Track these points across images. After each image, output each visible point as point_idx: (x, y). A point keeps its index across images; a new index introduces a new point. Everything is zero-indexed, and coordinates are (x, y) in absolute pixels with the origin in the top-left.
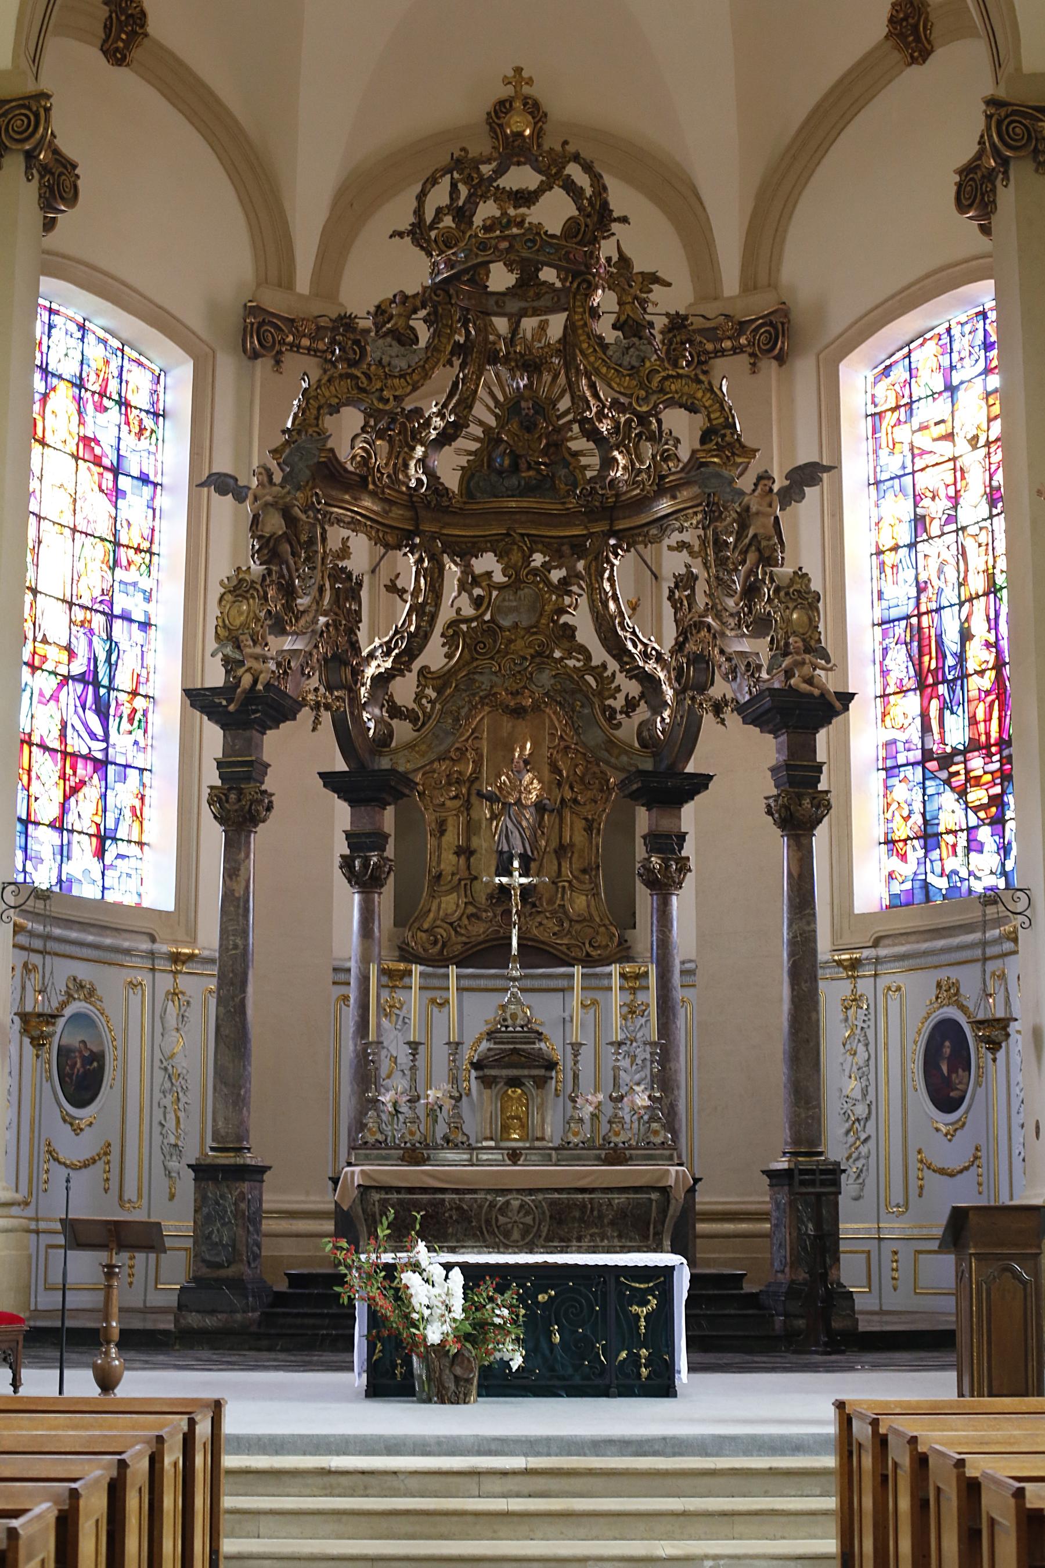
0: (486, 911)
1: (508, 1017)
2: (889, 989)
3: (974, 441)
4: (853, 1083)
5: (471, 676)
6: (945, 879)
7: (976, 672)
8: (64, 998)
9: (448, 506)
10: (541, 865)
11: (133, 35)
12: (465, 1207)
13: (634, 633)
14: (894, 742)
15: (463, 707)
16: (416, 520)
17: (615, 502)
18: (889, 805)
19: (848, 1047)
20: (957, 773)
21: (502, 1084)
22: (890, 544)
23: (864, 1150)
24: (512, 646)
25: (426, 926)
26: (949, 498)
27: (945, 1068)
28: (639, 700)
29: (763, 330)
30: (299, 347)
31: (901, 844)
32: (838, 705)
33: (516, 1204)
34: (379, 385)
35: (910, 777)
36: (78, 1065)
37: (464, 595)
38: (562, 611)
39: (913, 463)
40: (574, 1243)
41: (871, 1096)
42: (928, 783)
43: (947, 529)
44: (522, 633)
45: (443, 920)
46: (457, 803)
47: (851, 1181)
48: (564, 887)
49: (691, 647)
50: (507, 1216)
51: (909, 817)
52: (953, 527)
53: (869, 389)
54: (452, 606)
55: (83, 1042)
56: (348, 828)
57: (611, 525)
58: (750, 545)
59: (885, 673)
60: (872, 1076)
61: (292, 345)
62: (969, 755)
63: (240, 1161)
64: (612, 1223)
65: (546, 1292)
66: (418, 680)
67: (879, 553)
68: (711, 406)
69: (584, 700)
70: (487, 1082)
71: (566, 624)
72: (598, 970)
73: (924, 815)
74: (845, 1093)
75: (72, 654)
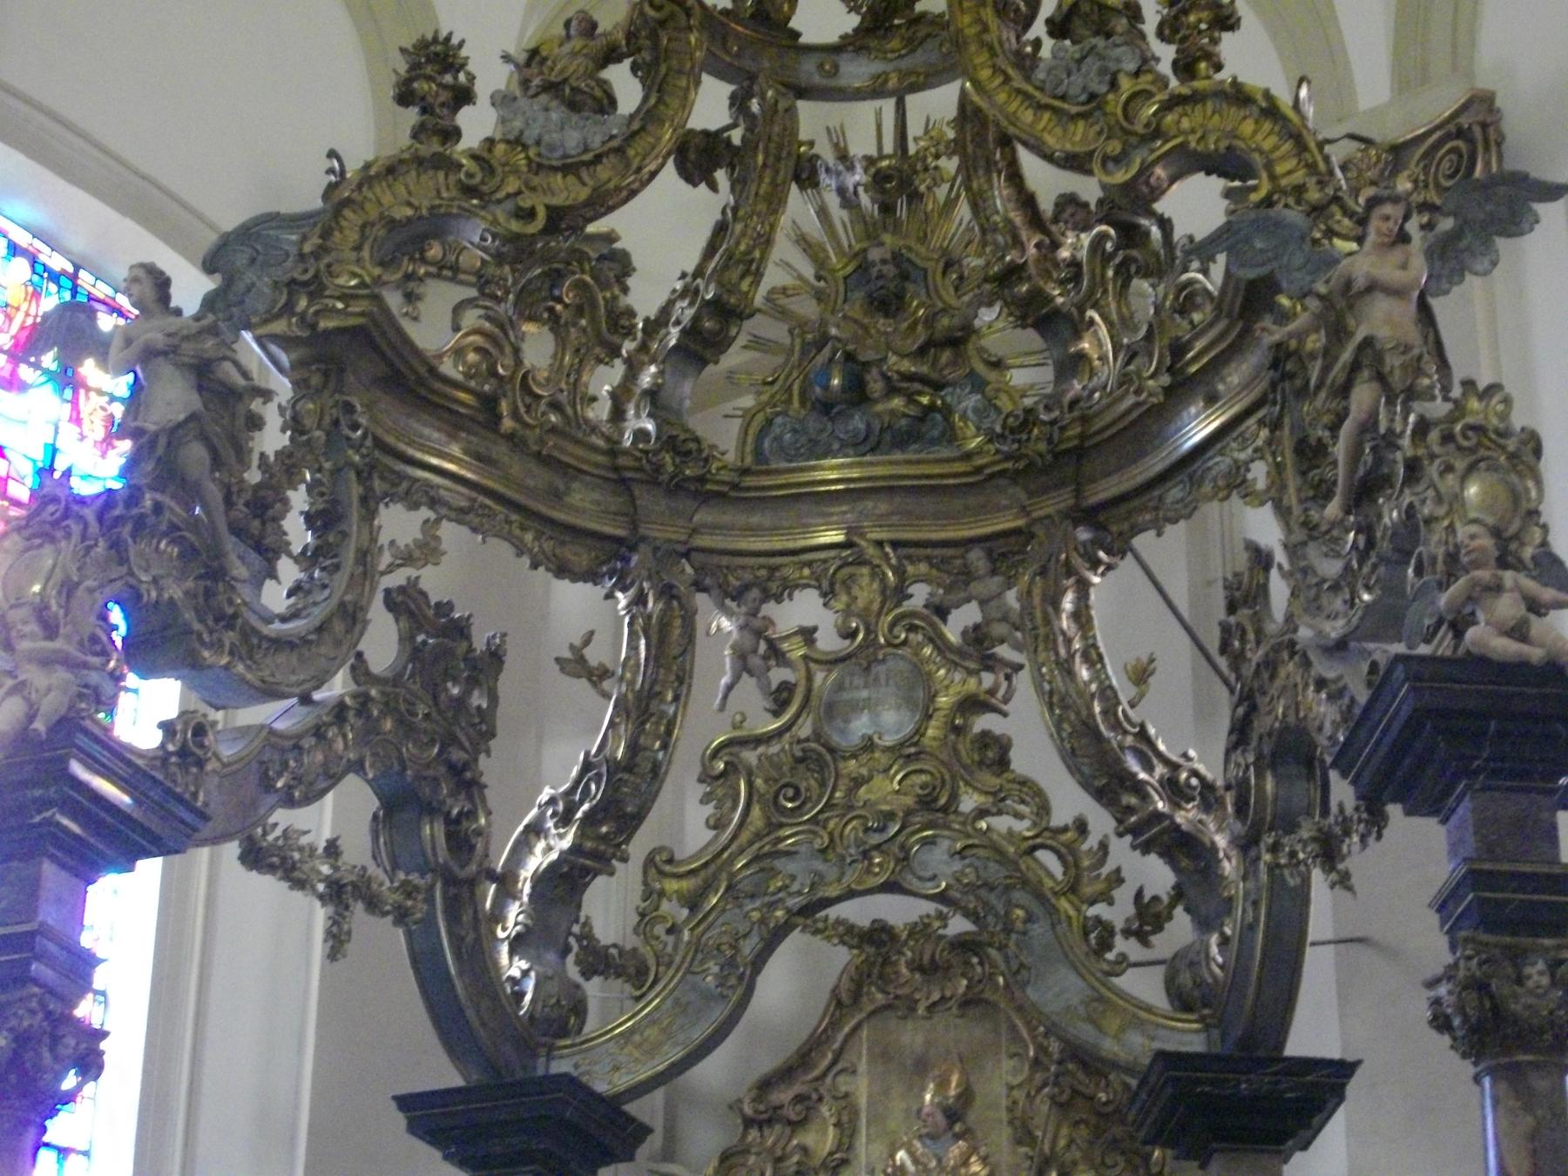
5: (766, 863)
9: (702, 480)
13: (1143, 735)
17: (1082, 437)
28: (1172, 906)
29: (1448, 146)
30: (455, 268)
34: (512, 185)
38: (973, 704)
44: (882, 759)
54: (722, 707)
57: (1078, 493)
58: (1355, 367)
61: (441, 265)
66: (645, 883)
68: (1276, 148)
69: (1037, 909)
71: (985, 734)
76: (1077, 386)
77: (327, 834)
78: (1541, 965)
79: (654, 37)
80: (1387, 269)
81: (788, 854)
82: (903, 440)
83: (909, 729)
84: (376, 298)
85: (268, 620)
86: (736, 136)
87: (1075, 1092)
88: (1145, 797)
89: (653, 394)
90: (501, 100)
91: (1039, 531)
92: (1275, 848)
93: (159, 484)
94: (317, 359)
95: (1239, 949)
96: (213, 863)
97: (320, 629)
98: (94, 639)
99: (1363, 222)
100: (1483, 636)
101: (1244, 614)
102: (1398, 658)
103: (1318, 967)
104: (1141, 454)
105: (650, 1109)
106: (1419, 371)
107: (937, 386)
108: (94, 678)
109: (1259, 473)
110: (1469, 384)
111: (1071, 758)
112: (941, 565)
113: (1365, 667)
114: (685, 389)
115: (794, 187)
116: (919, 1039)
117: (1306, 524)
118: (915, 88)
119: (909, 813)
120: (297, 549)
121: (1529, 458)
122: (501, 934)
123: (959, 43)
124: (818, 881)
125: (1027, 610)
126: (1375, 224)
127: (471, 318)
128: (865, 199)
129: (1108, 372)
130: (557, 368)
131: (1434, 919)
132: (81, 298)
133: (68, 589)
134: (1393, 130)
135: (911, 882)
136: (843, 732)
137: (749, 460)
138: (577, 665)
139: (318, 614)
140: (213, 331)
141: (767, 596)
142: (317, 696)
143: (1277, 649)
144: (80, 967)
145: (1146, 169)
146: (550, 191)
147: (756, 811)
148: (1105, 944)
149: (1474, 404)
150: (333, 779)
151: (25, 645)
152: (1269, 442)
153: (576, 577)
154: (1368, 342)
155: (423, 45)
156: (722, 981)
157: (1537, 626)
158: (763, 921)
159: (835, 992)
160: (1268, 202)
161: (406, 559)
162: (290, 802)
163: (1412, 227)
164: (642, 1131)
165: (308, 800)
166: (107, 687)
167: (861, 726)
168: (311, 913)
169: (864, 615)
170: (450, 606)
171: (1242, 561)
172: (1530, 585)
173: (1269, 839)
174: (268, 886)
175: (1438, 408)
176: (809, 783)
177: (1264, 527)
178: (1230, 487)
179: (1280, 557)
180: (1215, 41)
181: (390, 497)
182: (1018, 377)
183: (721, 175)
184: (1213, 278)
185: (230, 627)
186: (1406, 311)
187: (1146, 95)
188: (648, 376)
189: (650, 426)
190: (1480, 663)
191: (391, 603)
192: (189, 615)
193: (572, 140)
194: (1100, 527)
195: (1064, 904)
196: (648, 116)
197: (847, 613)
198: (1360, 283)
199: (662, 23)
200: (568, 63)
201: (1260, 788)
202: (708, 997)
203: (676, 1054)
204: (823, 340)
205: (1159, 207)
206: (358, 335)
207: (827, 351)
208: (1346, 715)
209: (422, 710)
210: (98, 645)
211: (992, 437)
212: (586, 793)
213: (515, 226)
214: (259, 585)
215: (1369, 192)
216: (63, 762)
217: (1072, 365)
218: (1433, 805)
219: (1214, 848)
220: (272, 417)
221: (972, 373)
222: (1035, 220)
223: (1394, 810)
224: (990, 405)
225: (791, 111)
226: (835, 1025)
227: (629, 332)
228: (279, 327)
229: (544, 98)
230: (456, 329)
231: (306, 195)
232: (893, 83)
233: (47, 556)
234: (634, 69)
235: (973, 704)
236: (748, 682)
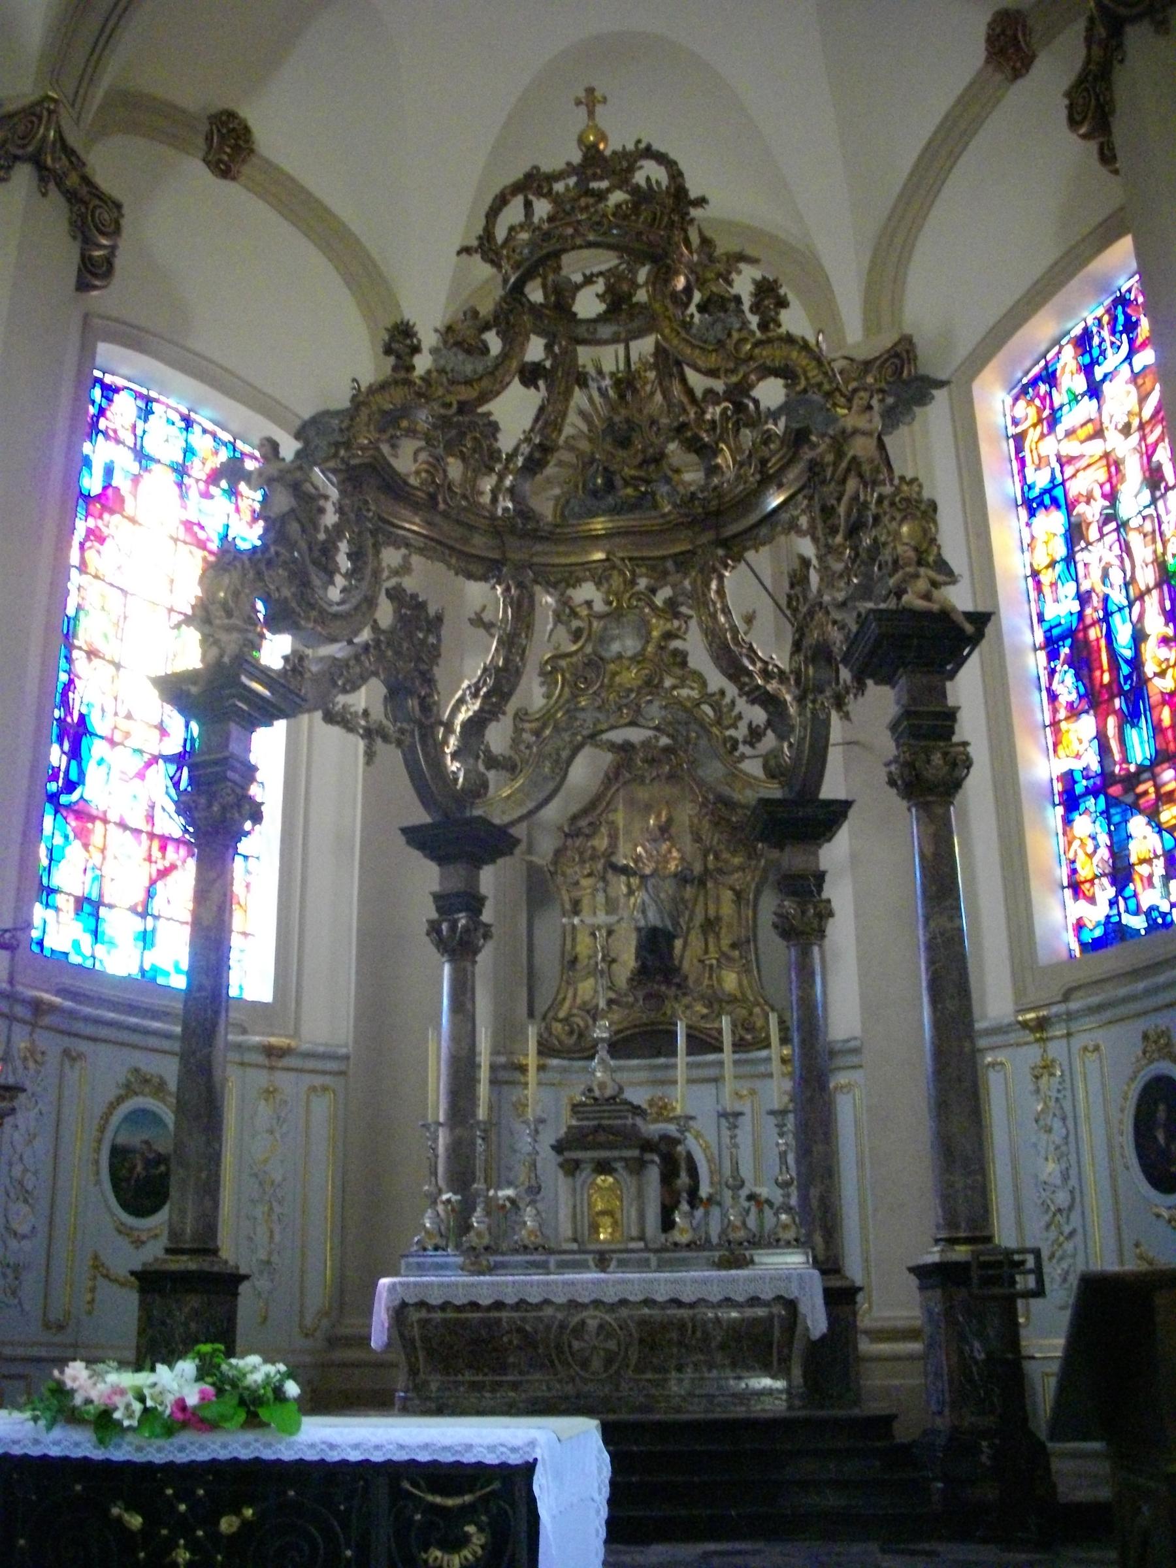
0: (626, 995)
2: (1085, 1049)
3: (1126, 430)
6: (1143, 917)
7: (1156, 674)
9: (536, 530)
13: (751, 648)
16: (502, 547)
18: (1070, 843)
19: (1042, 1123)
20: (1146, 793)
22: (1047, 561)
23: (1069, 1246)
26: (1104, 496)
27: (1161, 1137)
32: (969, 628)
33: (592, 1324)
34: (440, 392)
36: (139, 1168)
37: (561, 629)
38: (669, 636)
39: (1062, 472)
40: (674, 1374)
41: (1073, 1182)
42: (1112, 811)
43: (1106, 529)
44: (626, 663)
45: (579, 1008)
47: (1055, 1286)
49: (809, 641)
51: (1095, 852)
52: (1113, 525)
56: (436, 888)
58: (848, 470)
59: (1053, 697)
60: (1073, 1158)
62: (1158, 769)
63: (206, 1267)
64: (722, 1347)
65: (238, 1513)
73: (1110, 848)
75: (164, 732)
78: (939, 755)
80: (861, 422)
81: (583, 709)
83: (639, 648)
84: (378, 449)
86: (548, 364)
87: (720, 817)
90: (434, 351)
91: (700, 551)
92: (814, 701)
94: (349, 479)
95: (797, 749)
96: (311, 721)
98: (250, 618)
99: (850, 400)
100: (911, 599)
101: (798, 589)
102: (871, 611)
103: (835, 757)
105: (519, 831)
107: (648, 482)
108: (250, 636)
109: (804, 521)
110: (902, 478)
112: (653, 568)
113: (855, 614)
114: (527, 487)
115: (577, 389)
116: (647, 796)
117: (827, 545)
118: (635, 338)
119: (640, 688)
120: (343, 570)
121: (931, 512)
122: (447, 751)
123: (654, 318)
124: (597, 722)
126: (856, 401)
128: (611, 393)
129: (730, 474)
131: (889, 733)
132: (238, 455)
133: (236, 594)
134: (862, 354)
135: (641, 721)
136: (607, 650)
137: (558, 520)
138: (478, 621)
140: (300, 468)
141: (568, 586)
143: (813, 606)
144: (250, 772)
145: (746, 376)
147: (567, 690)
148: (735, 747)
149: (905, 488)
151: (218, 622)
152: (808, 506)
154: (854, 458)
157: (936, 594)
159: (607, 775)
160: (805, 391)
161: (396, 573)
162: (345, 691)
163: (875, 402)
164: (516, 842)
166: (256, 639)
167: (615, 647)
168: (356, 746)
169: (616, 594)
171: (796, 564)
172: (932, 574)
173: (811, 697)
174: (336, 731)
175: (887, 489)
176: (591, 675)
177: (807, 548)
179: (815, 562)
180: (777, 314)
182: (688, 477)
183: (541, 383)
184: (778, 428)
185: (313, 609)
186: (872, 443)
188: (508, 481)
189: (510, 505)
191: (389, 594)
192: (294, 605)
193: (468, 369)
195: (715, 730)
196: (505, 356)
197: (608, 593)
198: (849, 429)
199: (511, 311)
200: (466, 330)
202: (545, 779)
203: (531, 805)
204: (592, 461)
205: (755, 393)
208: (847, 638)
210: (252, 620)
211: (675, 506)
213: (442, 411)
214: (326, 589)
215: (854, 385)
216: (238, 676)
218: (888, 680)
220: (330, 508)
223: (870, 682)
224: (675, 490)
227: (499, 460)
231: (342, 401)
232: (623, 336)
235: (669, 636)
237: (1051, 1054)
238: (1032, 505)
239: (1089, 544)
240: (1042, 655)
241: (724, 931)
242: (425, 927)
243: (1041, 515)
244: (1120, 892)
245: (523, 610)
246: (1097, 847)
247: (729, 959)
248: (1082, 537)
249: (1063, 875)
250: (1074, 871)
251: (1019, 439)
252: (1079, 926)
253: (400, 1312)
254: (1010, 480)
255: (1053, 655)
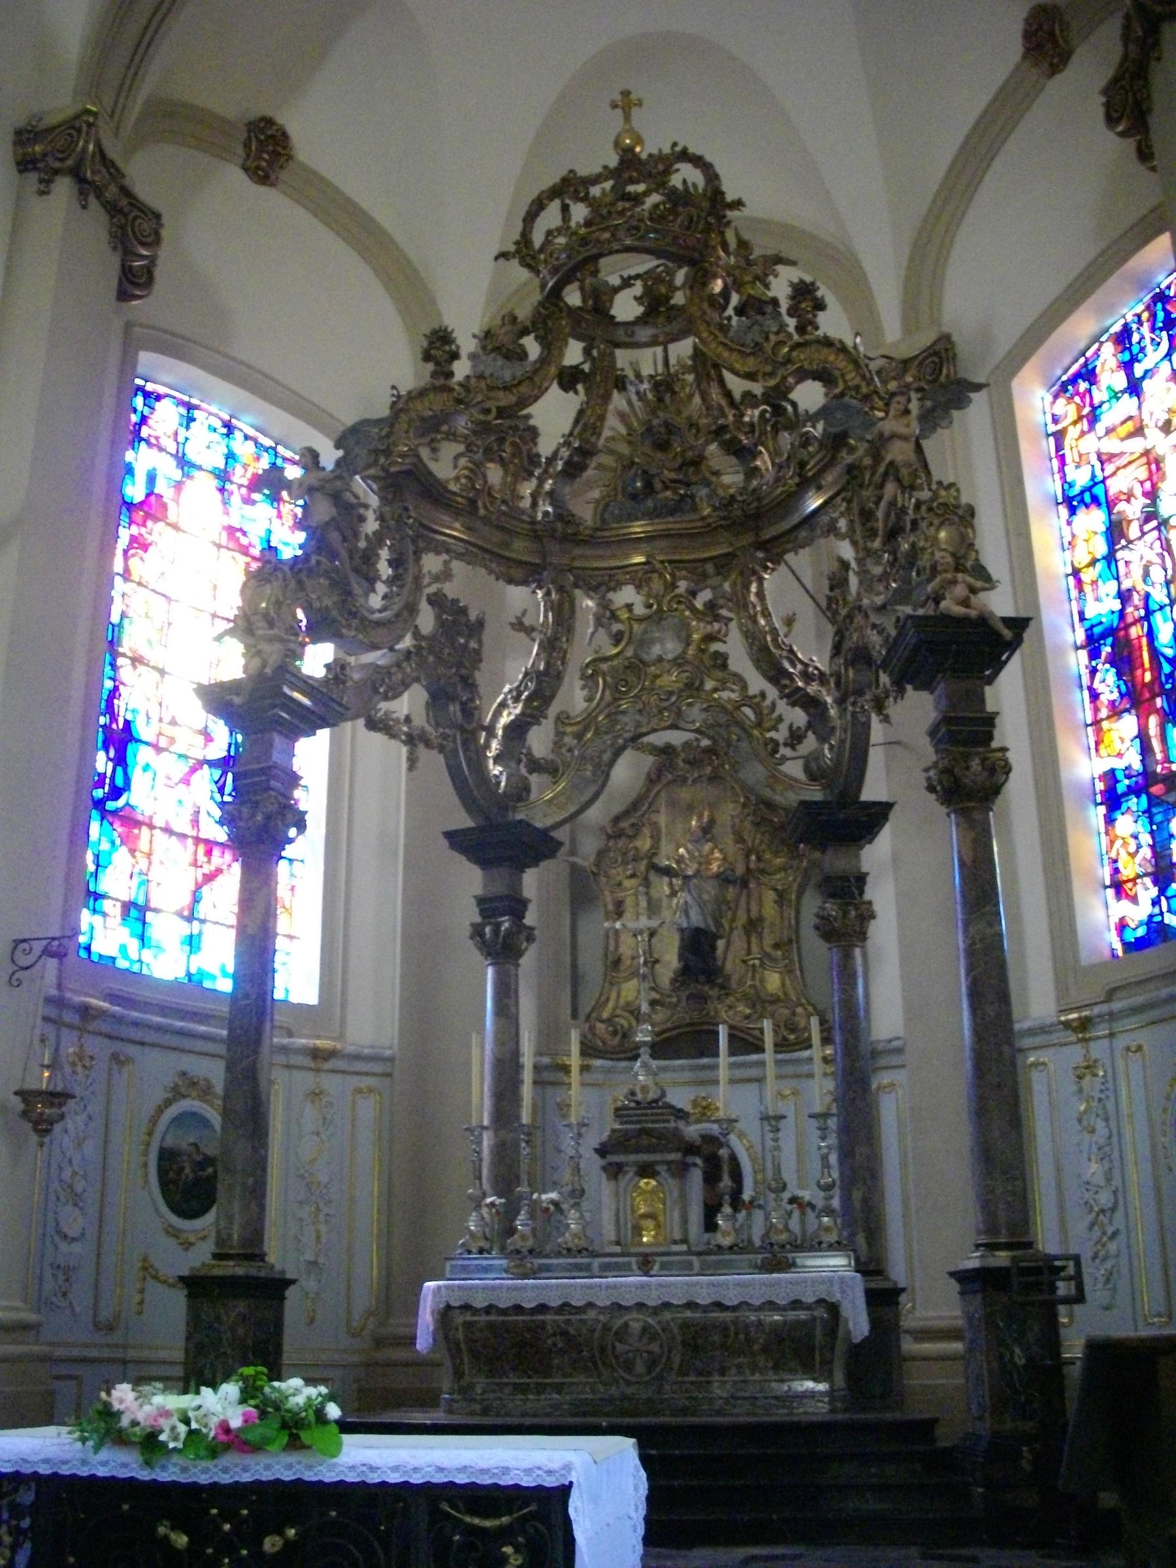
0: (670, 996)
1: (638, 1090)
2: (1128, 1049)
4: (1094, 1167)
8: (170, 1095)
9: (575, 534)
10: (728, 942)
11: (276, 155)
12: (572, 1332)
13: (791, 651)
14: (1112, 771)
15: (604, 751)
17: (758, 508)
18: (1112, 843)
19: (1085, 1123)
21: (631, 1174)
22: (1088, 559)
23: (1112, 1247)
24: (658, 682)
25: (605, 1015)
30: (454, 435)
31: (1130, 885)
32: (1007, 634)
33: (636, 1327)
34: (479, 398)
35: (1134, 808)
38: (710, 638)
41: (1117, 1181)
42: (1154, 810)
43: (1147, 528)
44: (668, 666)
45: (623, 1009)
46: (634, 882)
48: (754, 966)
50: (625, 1343)
51: (1137, 852)
52: (1154, 523)
53: (1047, 409)
55: (195, 1145)
59: (1095, 696)
60: (1116, 1155)
64: (766, 1350)
67: (1076, 573)
69: (744, 736)
70: (614, 1171)
72: (796, 1055)
74: (1084, 1178)
76: (755, 483)
77: (406, 712)
79: (545, 323)
82: (673, 511)
84: (418, 456)
85: (373, 612)
86: (586, 367)
88: (792, 680)
89: (551, 494)
90: (473, 357)
92: (854, 704)
93: (319, 550)
94: (391, 486)
95: (838, 751)
96: (354, 729)
97: (397, 615)
98: (292, 628)
99: (887, 405)
101: (837, 592)
102: (909, 617)
103: (876, 758)
104: (783, 517)
105: (561, 835)
106: (916, 476)
107: (688, 485)
108: (292, 646)
109: (842, 524)
110: (940, 483)
111: (757, 663)
112: (692, 571)
113: (894, 619)
115: (615, 392)
119: (681, 691)
120: (384, 577)
123: (690, 321)
124: (638, 725)
125: (734, 593)
127: (463, 462)
128: (650, 396)
130: (504, 483)
131: (927, 740)
133: (278, 604)
134: (904, 352)
135: (682, 724)
138: (519, 626)
139: (396, 608)
140: (340, 477)
141: (609, 590)
142: (397, 647)
143: (852, 609)
144: (294, 780)
145: (784, 378)
146: (498, 400)
147: (607, 693)
148: (775, 751)
149: (943, 493)
150: (406, 686)
151: (260, 632)
153: (518, 584)
154: (892, 463)
155: (435, 332)
156: (594, 773)
158: (612, 745)
159: (648, 774)
160: (842, 395)
162: (386, 698)
165: (395, 697)
166: (298, 649)
167: (656, 650)
169: (656, 597)
170: (458, 601)
171: (835, 566)
173: (852, 699)
174: (378, 738)
175: (925, 495)
176: (632, 678)
177: (846, 551)
178: (829, 531)
179: (854, 565)
180: (815, 316)
181: (427, 550)
182: (726, 479)
183: (580, 387)
184: (818, 430)
186: (909, 447)
187: (782, 343)
189: (550, 509)
190: (947, 619)
193: (507, 375)
194: (766, 550)
195: (756, 732)
196: (543, 361)
198: (887, 434)
199: (549, 316)
201: (847, 676)
204: (633, 463)
205: (792, 396)
206: (408, 473)
207: (633, 470)
209: (447, 651)
211: (715, 509)
212: (526, 688)
213: (482, 417)
214: (367, 596)
217: (752, 472)
218: (926, 685)
219: (825, 703)
220: (370, 516)
221: (705, 478)
222: (732, 403)
223: (909, 687)
224: (714, 492)
225: (612, 355)
226: (649, 790)
227: (538, 464)
228: (372, 471)
229: (493, 355)
230: (455, 467)
231: (382, 410)
233: (268, 590)
234: (536, 338)
235: (710, 638)
236: (601, 630)
237: (1094, 1055)
238: (1073, 503)
239: (1130, 542)
240: (1083, 655)
241: (766, 931)
242: (468, 931)
243: (1082, 513)
244: (1162, 892)
245: (564, 615)
246: (1139, 847)
247: (773, 960)
248: (1123, 535)
249: (1106, 874)
250: (1116, 871)
251: (1059, 436)
252: (1122, 926)
253: (445, 1315)
254: (1050, 479)
255: (1094, 654)
